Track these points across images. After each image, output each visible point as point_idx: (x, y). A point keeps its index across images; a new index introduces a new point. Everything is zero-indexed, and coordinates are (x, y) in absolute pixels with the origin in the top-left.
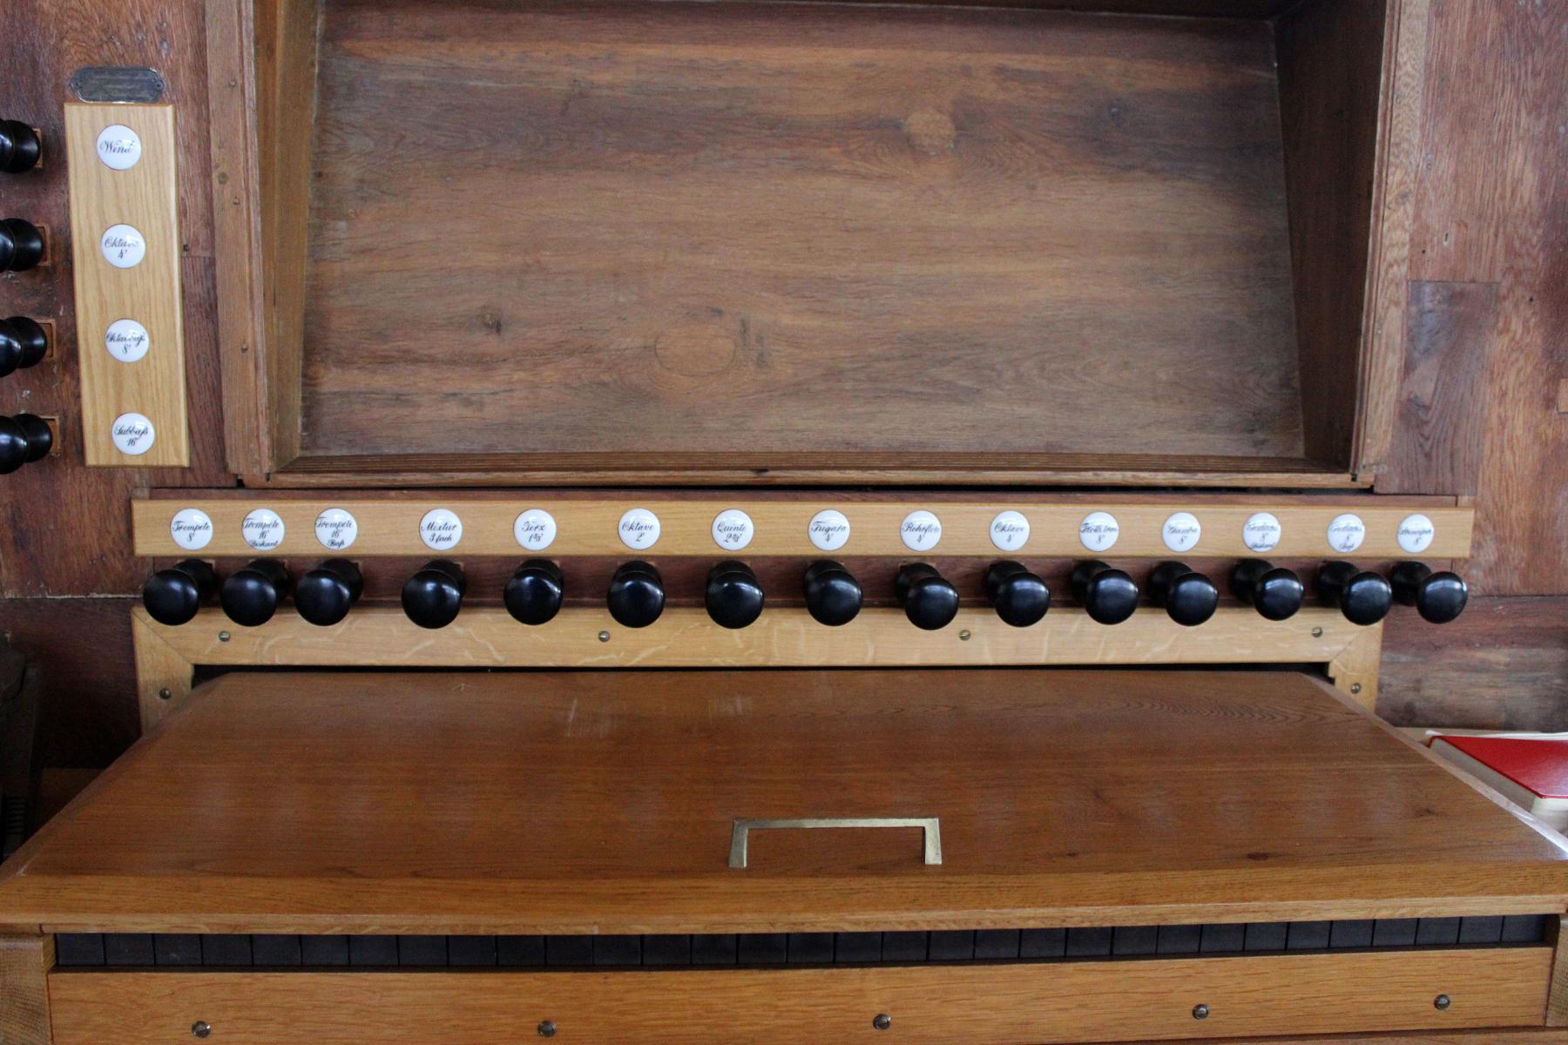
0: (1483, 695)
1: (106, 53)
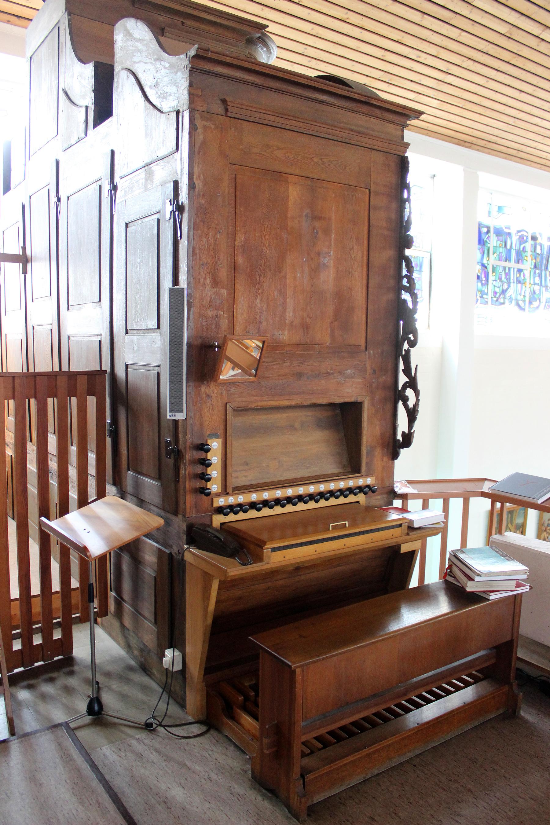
0: (377, 503)
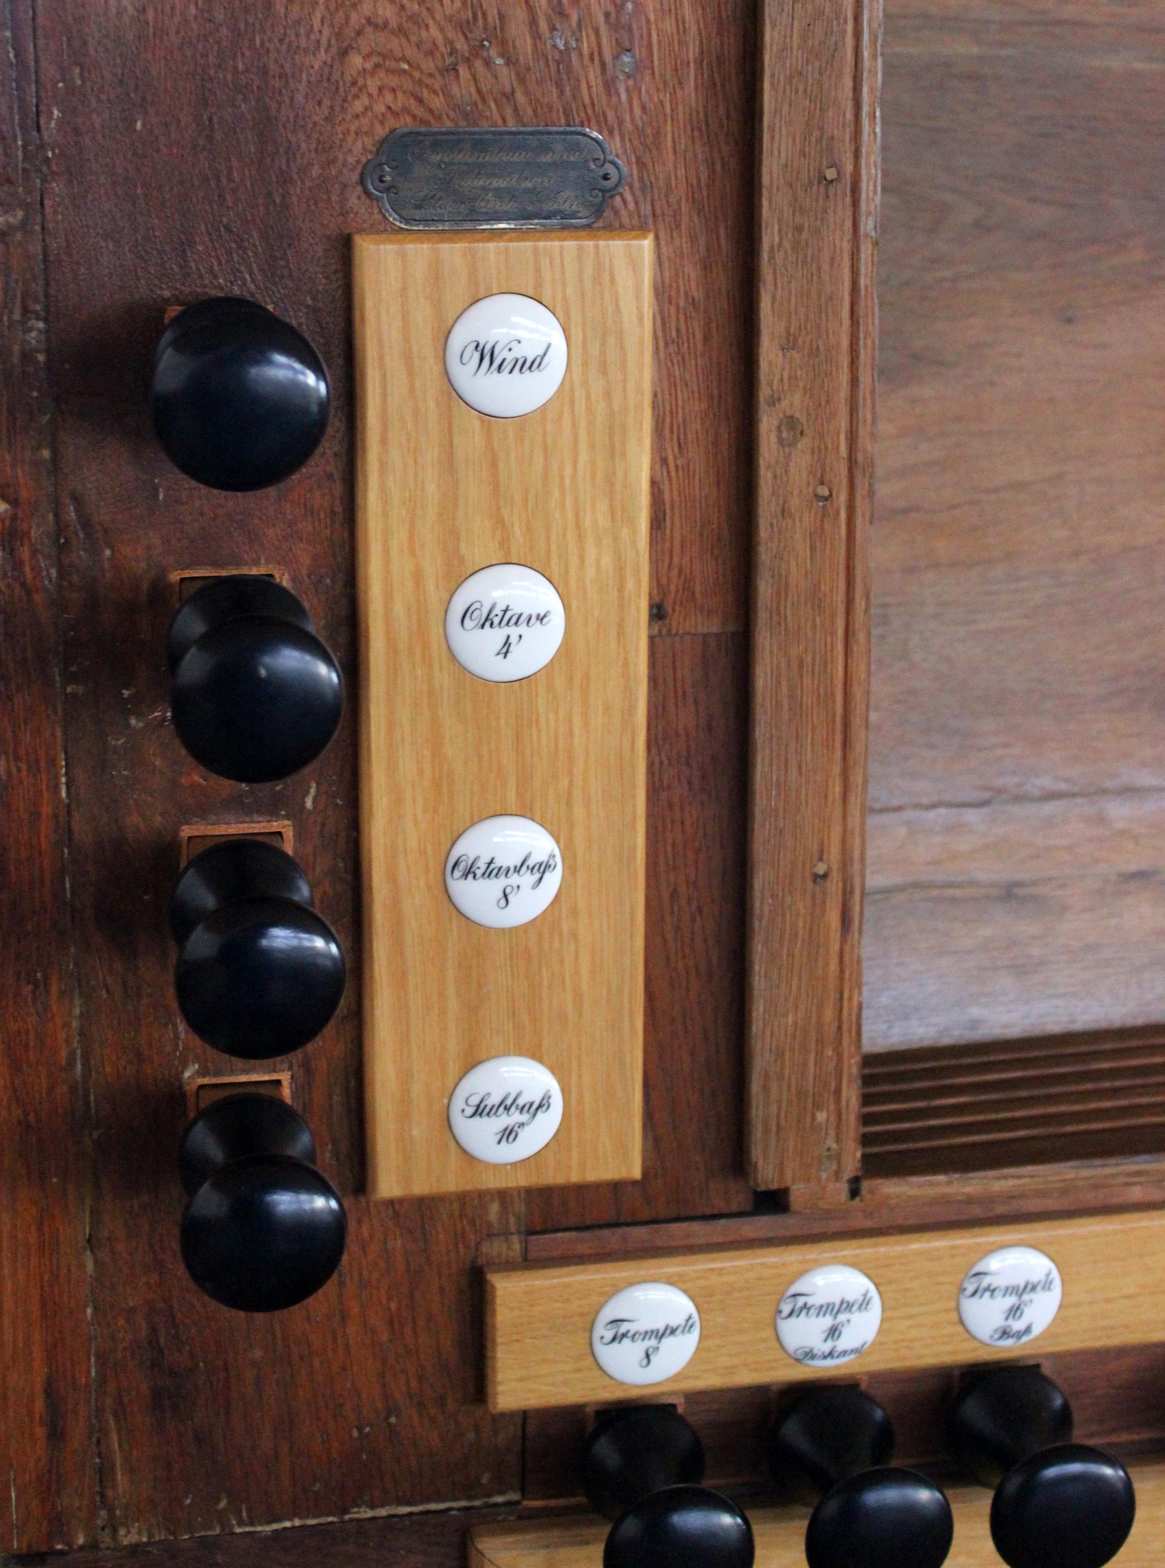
1: (463, 88)
